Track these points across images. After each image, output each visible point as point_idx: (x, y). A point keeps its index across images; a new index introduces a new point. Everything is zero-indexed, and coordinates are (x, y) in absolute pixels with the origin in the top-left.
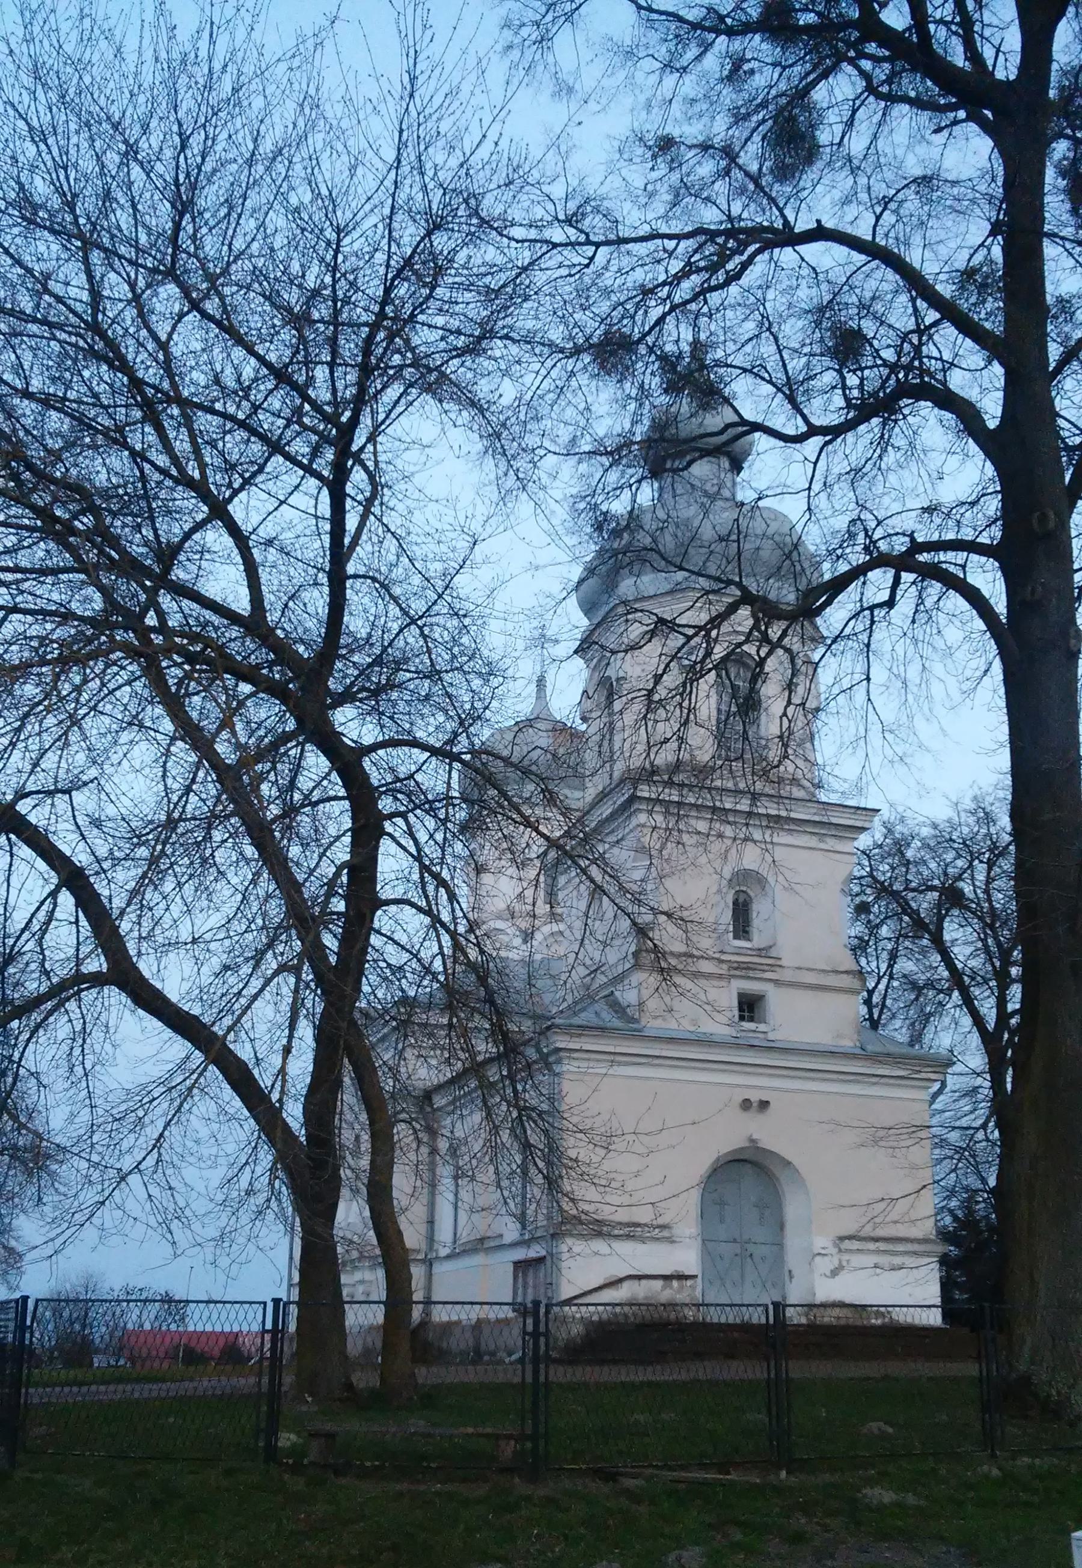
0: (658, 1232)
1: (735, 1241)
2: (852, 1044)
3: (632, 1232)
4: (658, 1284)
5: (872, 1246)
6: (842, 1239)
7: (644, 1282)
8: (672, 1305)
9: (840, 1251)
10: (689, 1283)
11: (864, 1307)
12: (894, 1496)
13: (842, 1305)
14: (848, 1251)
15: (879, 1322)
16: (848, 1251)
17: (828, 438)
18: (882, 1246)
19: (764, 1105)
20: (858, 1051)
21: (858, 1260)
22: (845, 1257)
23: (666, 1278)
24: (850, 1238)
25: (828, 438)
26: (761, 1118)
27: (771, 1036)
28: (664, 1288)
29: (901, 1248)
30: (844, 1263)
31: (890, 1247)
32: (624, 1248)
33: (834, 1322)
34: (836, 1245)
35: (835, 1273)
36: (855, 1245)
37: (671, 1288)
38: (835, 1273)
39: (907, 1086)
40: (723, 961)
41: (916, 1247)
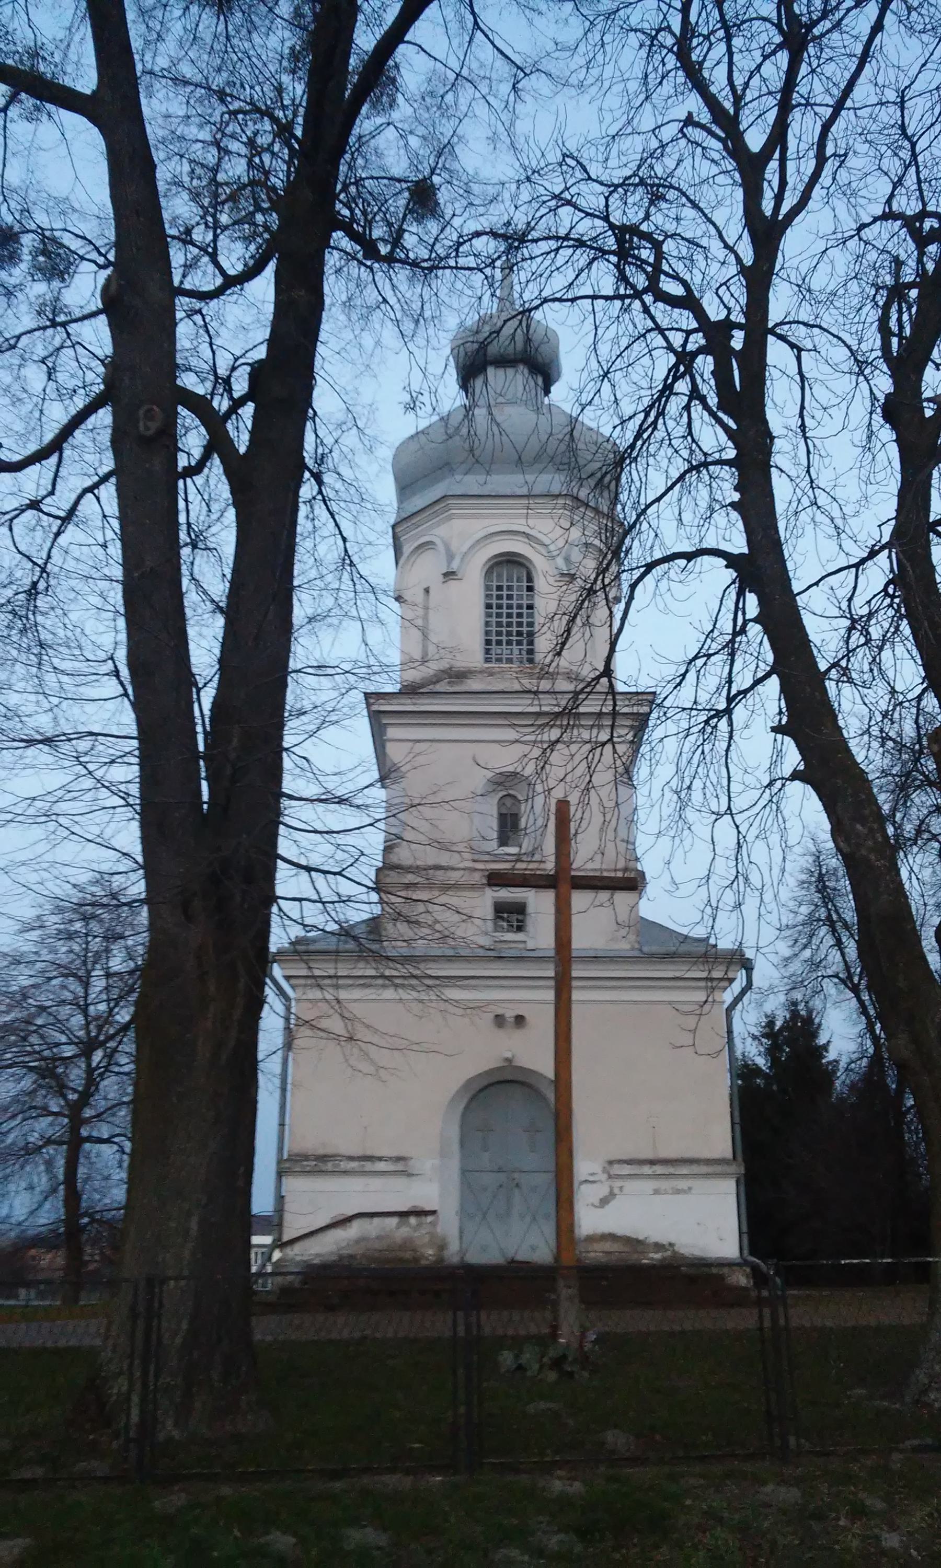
0: (401, 1166)
1: (500, 1171)
2: (628, 947)
3: (364, 1163)
4: (394, 1221)
5: (647, 1170)
6: (611, 1163)
7: (376, 1220)
8: (407, 1244)
9: (610, 1177)
10: (430, 1219)
11: (638, 1241)
12: (885, 1535)
13: (612, 1237)
14: (619, 1177)
15: (658, 1256)
16: (619, 1177)
17: (777, 155)
18: (659, 1169)
19: (520, 1020)
20: (636, 953)
21: (631, 1186)
22: (617, 1183)
23: (403, 1215)
24: (621, 1162)
25: (777, 155)
26: (518, 1034)
27: (530, 945)
28: (398, 1226)
29: (685, 1170)
30: (616, 1191)
31: (671, 1170)
32: (355, 1184)
33: (604, 1259)
34: (605, 1170)
35: (604, 1202)
36: (626, 1170)
37: (409, 1225)
38: (604, 1202)
39: (679, 988)
40: (476, 870)
41: (704, 1169)
